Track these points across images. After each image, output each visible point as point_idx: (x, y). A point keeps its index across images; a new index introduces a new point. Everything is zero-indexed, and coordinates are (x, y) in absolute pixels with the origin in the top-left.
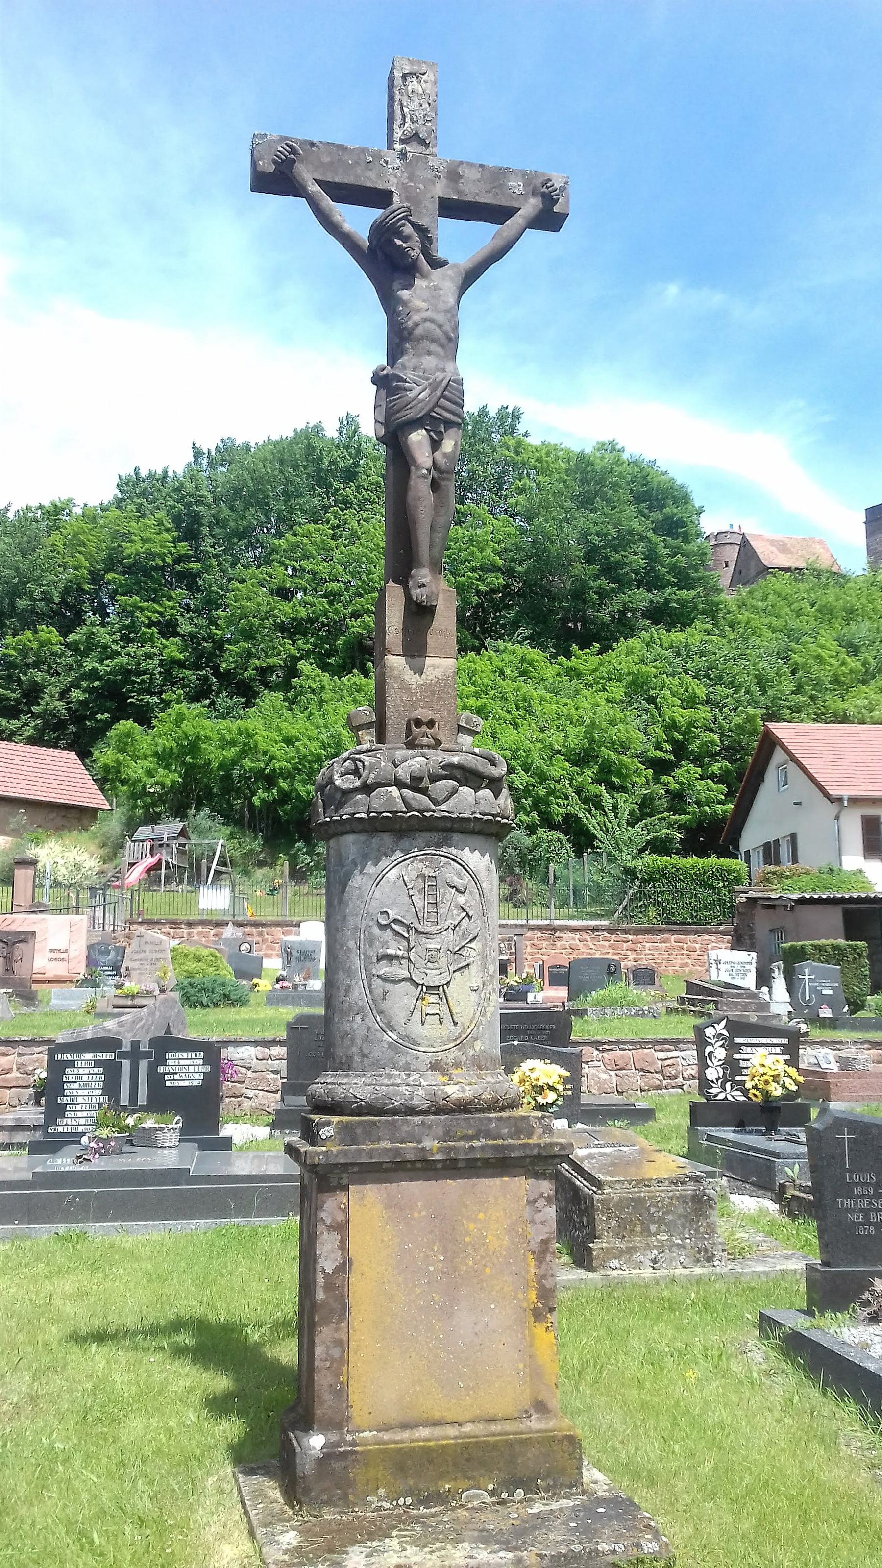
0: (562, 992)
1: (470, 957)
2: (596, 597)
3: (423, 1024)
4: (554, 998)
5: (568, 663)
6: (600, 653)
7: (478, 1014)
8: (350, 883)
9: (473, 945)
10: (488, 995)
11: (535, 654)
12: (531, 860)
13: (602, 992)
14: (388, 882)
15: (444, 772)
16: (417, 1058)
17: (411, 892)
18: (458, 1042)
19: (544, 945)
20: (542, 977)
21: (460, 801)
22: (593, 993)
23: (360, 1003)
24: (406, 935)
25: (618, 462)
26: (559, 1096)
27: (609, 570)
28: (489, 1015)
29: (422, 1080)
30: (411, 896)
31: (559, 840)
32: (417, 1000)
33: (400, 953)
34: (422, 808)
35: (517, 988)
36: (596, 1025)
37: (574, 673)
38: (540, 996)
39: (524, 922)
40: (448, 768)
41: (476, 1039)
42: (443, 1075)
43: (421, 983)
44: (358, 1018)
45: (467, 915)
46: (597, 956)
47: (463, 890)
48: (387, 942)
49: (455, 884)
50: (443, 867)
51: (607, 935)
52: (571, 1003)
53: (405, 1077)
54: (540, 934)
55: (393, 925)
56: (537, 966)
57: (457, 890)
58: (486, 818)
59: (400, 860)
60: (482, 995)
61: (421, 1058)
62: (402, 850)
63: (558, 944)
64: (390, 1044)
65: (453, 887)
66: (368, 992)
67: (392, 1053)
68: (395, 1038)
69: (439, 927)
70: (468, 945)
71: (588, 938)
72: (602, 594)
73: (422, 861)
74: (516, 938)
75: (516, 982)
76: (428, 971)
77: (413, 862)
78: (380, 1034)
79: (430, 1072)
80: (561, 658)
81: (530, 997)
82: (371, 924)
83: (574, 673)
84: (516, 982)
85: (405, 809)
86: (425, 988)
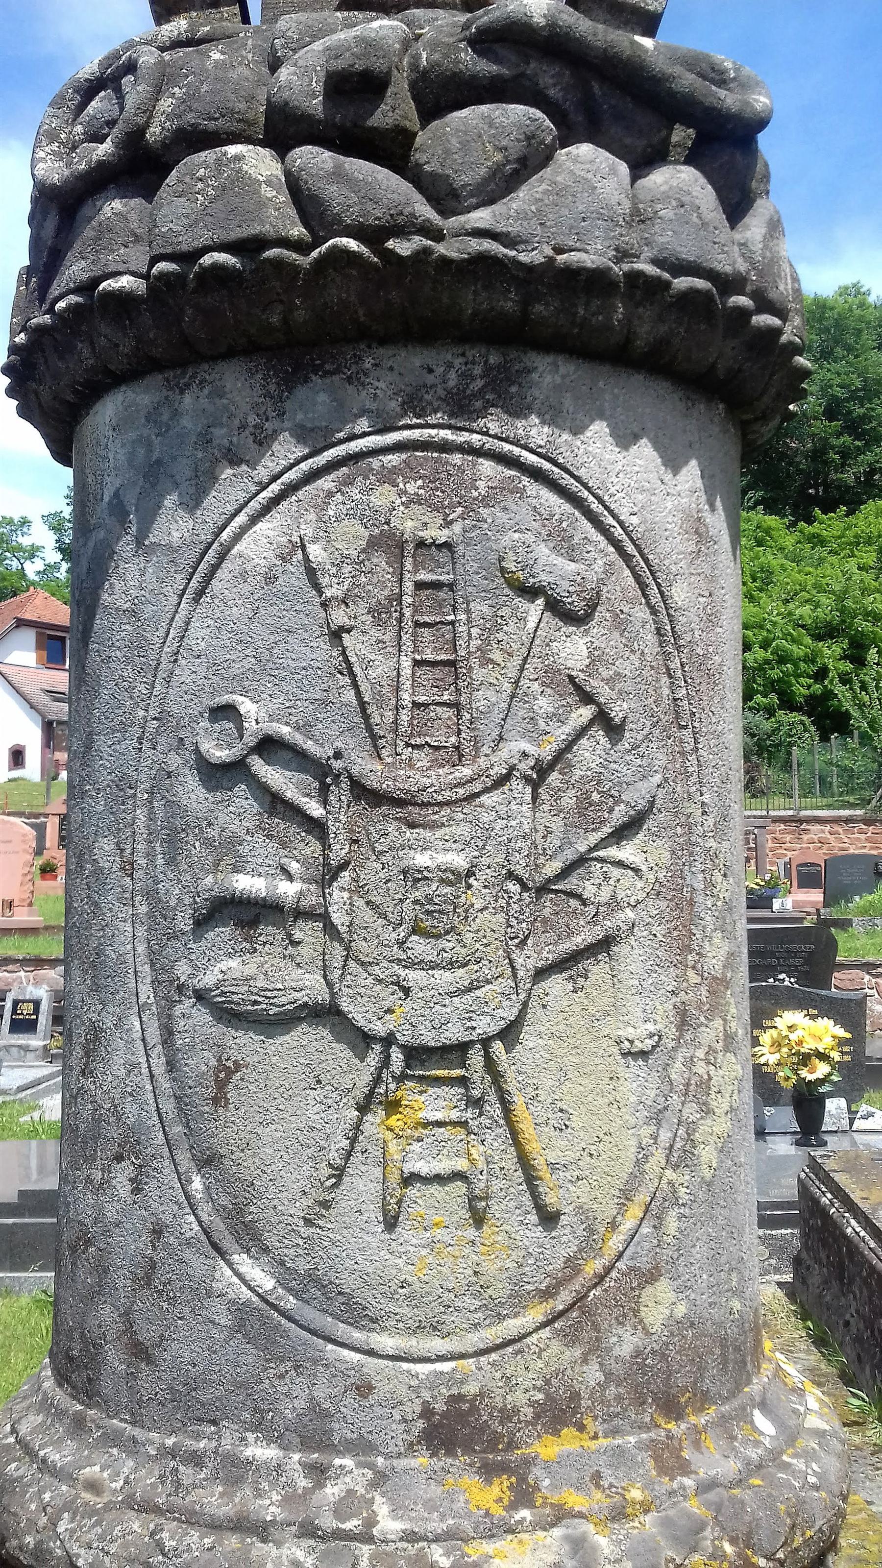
0: (816, 896)
1: (615, 904)
2: (837, 457)
3: (391, 1223)
4: (804, 902)
5: (809, 529)
6: (847, 516)
7: (658, 1156)
8: (106, 598)
9: (627, 852)
10: (701, 1068)
11: (772, 521)
12: (771, 745)
13: (870, 898)
14: (243, 575)
15: (485, 67)
16: (364, 1389)
17: (339, 616)
18: (564, 1298)
19: (788, 839)
20: (788, 875)
21: (560, 192)
22: (857, 898)
23: (130, 1109)
24: (315, 810)
25: (862, 305)
26: (833, 1068)
27: (854, 427)
28: (707, 1154)
29: (382, 1508)
30: (336, 635)
31: (802, 723)
32: (363, 1108)
33: (288, 890)
34: (376, 214)
35: (759, 893)
36: (864, 940)
37: (817, 540)
38: (789, 903)
39: (764, 813)
40: (502, 50)
41: (651, 1276)
42: (489, 1471)
43: (380, 1028)
44: (122, 1175)
45: (602, 718)
46: (851, 851)
47: (578, 605)
48: (234, 841)
49: (544, 578)
50: (485, 501)
51: (863, 826)
52: (828, 910)
53: (303, 1483)
54: (782, 827)
55: (258, 765)
56: (781, 862)
57: (555, 607)
58: (682, 283)
59: (291, 475)
60: (677, 1072)
61: (383, 1389)
62: (301, 434)
63: (805, 837)
64: (240, 1310)
65: (530, 592)
66: (159, 1065)
67: (250, 1356)
68: (268, 1283)
69: (467, 772)
70: (613, 852)
71: (841, 830)
72: (846, 454)
73: (388, 477)
74: (756, 831)
75: (757, 884)
76: (414, 977)
77: (348, 482)
78: (197, 1264)
79: (422, 1460)
80: (802, 524)
81: (776, 904)
82: (174, 761)
83: (817, 540)
84: (757, 884)
85: (297, 231)
86: (397, 1056)
